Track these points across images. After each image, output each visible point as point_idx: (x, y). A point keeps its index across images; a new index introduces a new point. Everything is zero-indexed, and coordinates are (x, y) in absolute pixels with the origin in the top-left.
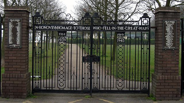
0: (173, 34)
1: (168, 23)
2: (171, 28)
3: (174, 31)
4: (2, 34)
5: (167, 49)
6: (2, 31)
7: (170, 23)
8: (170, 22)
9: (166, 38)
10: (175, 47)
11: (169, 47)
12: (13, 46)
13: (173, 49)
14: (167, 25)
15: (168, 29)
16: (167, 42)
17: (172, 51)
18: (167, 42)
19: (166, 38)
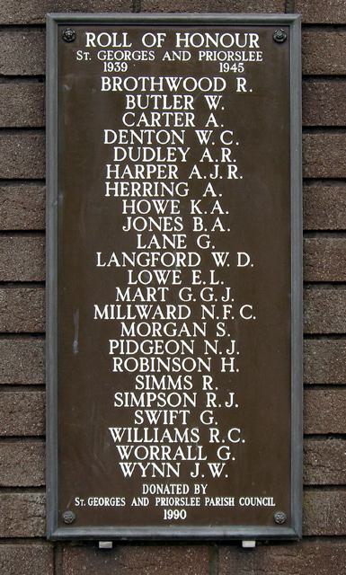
0: (244, 259)
1: (137, 69)
2: (196, 149)
3: (250, 215)
4: (106, 502)
5: (118, 542)
6: (230, 502)
7: (175, 69)
8: (185, 39)
9: (113, 328)
10: (282, 503)
11: (174, 504)
12: (153, 514)
13: (248, 533)
14: (118, 99)
15: (140, 181)
16: (125, 417)
17: (226, 556)
18: (125, 417)
19: (113, 328)
